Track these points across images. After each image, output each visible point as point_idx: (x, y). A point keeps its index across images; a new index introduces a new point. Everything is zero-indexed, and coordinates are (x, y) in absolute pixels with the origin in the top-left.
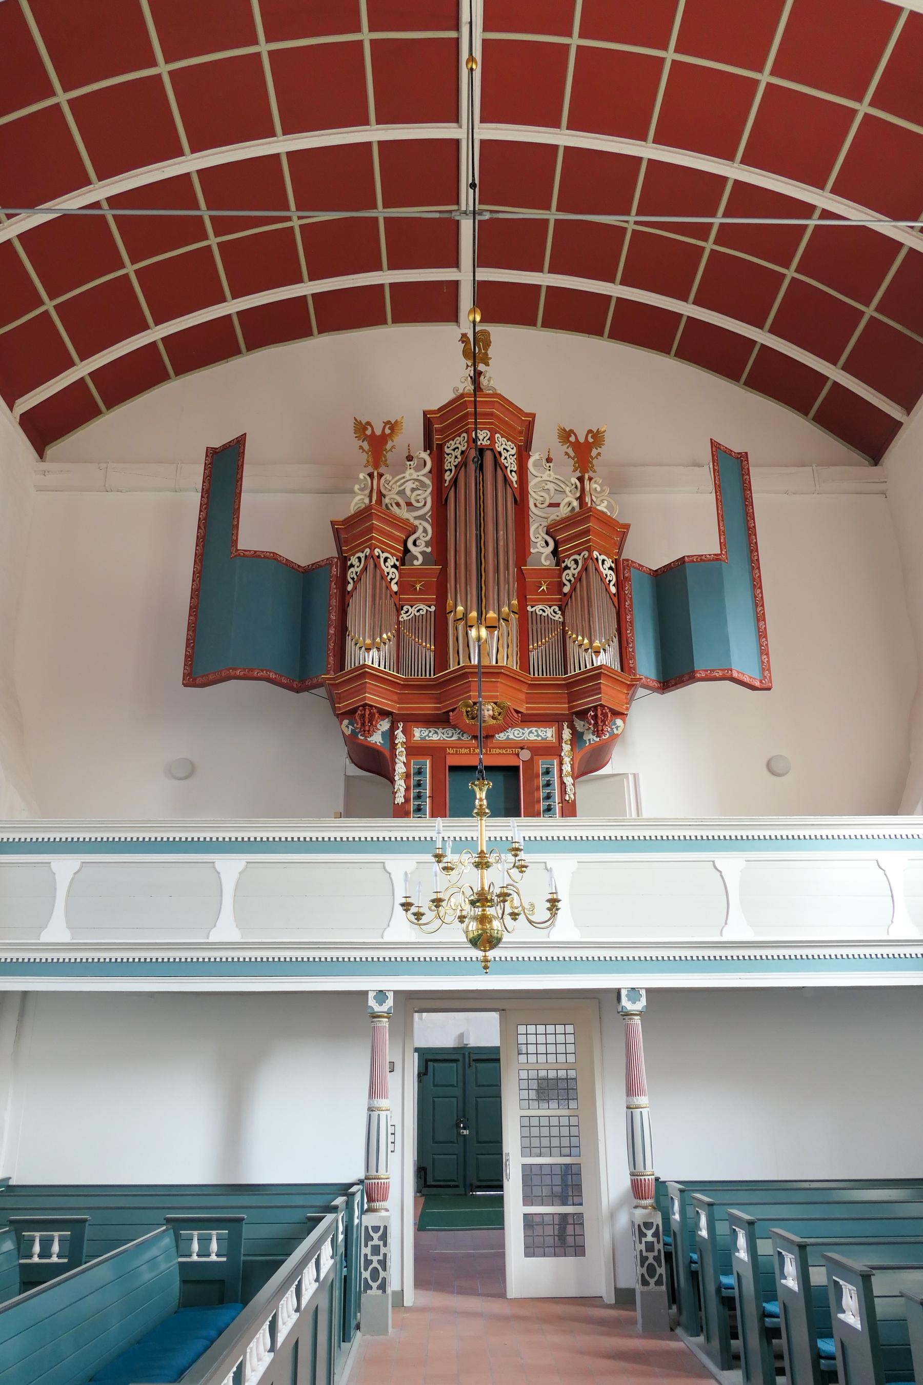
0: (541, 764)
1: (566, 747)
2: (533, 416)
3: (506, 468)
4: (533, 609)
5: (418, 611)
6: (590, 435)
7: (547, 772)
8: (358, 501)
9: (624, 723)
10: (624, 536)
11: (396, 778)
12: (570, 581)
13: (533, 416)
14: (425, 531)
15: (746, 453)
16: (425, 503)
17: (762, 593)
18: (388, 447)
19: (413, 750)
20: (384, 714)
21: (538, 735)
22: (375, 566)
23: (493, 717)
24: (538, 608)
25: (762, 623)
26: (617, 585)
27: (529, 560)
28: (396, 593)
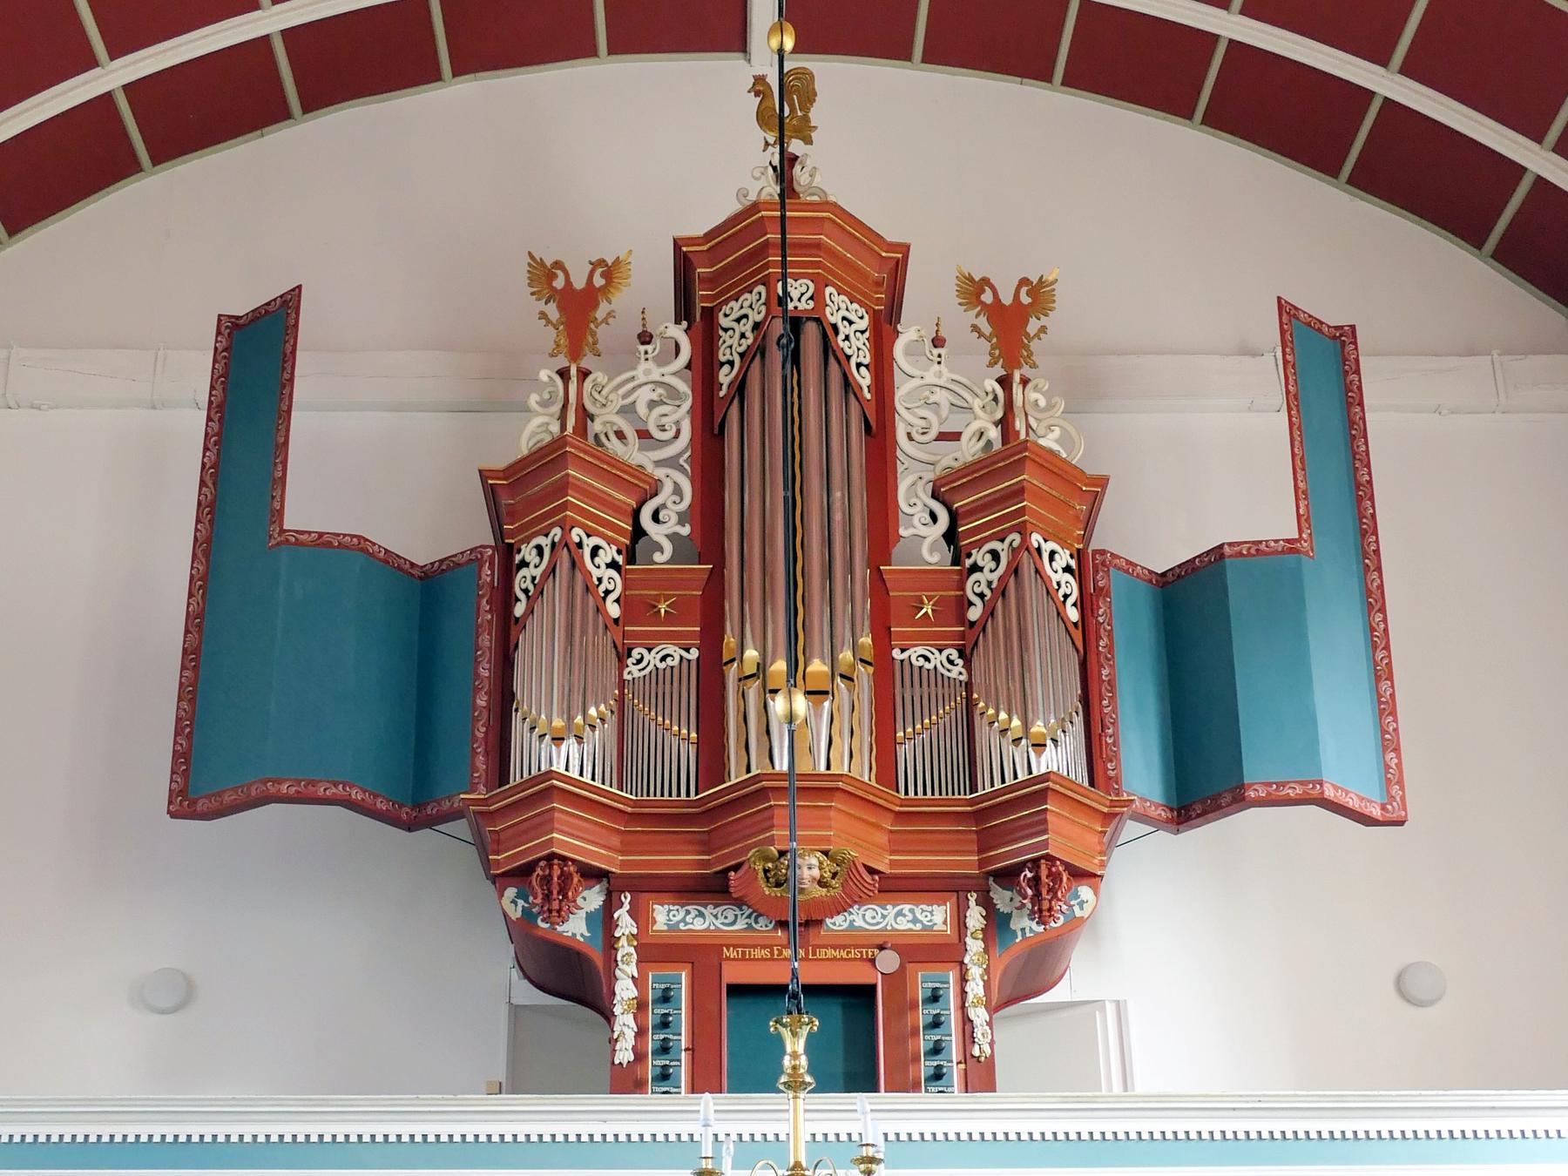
0: (922, 980)
1: (975, 946)
2: (905, 249)
3: (848, 357)
4: (905, 655)
5: (663, 659)
6: (1024, 290)
7: (934, 998)
8: (536, 427)
9: (1096, 893)
10: (1095, 501)
11: (617, 1010)
12: (981, 596)
13: (905, 249)
14: (677, 490)
15: (1353, 327)
16: (676, 437)
17: (1385, 620)
18: (600, 314)
19: (653, 952)
20: (592, 875)
21: (915, 921)
22: (573, 564)
23: (821, 883)
24: (914, 653)
25: (1385, 685)
26: (1081, 604)
27: (897, 551)
28: (616, 621)
